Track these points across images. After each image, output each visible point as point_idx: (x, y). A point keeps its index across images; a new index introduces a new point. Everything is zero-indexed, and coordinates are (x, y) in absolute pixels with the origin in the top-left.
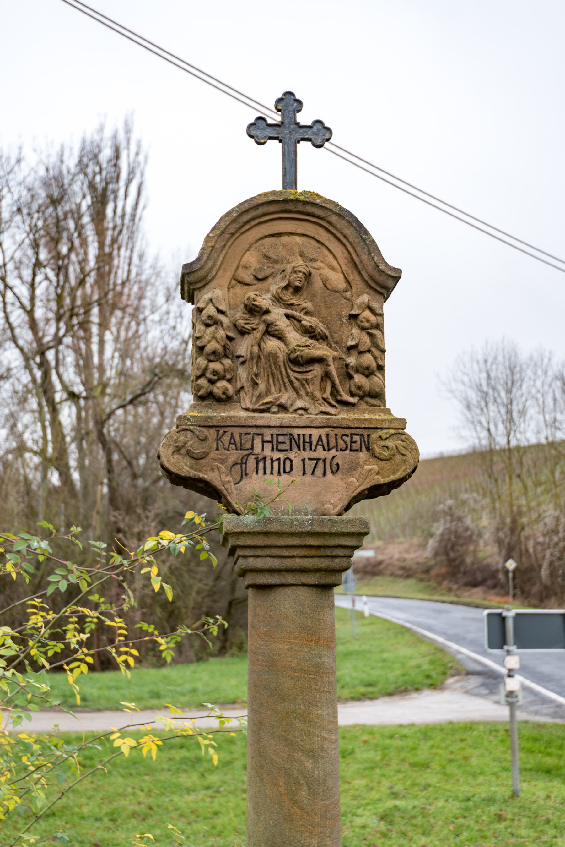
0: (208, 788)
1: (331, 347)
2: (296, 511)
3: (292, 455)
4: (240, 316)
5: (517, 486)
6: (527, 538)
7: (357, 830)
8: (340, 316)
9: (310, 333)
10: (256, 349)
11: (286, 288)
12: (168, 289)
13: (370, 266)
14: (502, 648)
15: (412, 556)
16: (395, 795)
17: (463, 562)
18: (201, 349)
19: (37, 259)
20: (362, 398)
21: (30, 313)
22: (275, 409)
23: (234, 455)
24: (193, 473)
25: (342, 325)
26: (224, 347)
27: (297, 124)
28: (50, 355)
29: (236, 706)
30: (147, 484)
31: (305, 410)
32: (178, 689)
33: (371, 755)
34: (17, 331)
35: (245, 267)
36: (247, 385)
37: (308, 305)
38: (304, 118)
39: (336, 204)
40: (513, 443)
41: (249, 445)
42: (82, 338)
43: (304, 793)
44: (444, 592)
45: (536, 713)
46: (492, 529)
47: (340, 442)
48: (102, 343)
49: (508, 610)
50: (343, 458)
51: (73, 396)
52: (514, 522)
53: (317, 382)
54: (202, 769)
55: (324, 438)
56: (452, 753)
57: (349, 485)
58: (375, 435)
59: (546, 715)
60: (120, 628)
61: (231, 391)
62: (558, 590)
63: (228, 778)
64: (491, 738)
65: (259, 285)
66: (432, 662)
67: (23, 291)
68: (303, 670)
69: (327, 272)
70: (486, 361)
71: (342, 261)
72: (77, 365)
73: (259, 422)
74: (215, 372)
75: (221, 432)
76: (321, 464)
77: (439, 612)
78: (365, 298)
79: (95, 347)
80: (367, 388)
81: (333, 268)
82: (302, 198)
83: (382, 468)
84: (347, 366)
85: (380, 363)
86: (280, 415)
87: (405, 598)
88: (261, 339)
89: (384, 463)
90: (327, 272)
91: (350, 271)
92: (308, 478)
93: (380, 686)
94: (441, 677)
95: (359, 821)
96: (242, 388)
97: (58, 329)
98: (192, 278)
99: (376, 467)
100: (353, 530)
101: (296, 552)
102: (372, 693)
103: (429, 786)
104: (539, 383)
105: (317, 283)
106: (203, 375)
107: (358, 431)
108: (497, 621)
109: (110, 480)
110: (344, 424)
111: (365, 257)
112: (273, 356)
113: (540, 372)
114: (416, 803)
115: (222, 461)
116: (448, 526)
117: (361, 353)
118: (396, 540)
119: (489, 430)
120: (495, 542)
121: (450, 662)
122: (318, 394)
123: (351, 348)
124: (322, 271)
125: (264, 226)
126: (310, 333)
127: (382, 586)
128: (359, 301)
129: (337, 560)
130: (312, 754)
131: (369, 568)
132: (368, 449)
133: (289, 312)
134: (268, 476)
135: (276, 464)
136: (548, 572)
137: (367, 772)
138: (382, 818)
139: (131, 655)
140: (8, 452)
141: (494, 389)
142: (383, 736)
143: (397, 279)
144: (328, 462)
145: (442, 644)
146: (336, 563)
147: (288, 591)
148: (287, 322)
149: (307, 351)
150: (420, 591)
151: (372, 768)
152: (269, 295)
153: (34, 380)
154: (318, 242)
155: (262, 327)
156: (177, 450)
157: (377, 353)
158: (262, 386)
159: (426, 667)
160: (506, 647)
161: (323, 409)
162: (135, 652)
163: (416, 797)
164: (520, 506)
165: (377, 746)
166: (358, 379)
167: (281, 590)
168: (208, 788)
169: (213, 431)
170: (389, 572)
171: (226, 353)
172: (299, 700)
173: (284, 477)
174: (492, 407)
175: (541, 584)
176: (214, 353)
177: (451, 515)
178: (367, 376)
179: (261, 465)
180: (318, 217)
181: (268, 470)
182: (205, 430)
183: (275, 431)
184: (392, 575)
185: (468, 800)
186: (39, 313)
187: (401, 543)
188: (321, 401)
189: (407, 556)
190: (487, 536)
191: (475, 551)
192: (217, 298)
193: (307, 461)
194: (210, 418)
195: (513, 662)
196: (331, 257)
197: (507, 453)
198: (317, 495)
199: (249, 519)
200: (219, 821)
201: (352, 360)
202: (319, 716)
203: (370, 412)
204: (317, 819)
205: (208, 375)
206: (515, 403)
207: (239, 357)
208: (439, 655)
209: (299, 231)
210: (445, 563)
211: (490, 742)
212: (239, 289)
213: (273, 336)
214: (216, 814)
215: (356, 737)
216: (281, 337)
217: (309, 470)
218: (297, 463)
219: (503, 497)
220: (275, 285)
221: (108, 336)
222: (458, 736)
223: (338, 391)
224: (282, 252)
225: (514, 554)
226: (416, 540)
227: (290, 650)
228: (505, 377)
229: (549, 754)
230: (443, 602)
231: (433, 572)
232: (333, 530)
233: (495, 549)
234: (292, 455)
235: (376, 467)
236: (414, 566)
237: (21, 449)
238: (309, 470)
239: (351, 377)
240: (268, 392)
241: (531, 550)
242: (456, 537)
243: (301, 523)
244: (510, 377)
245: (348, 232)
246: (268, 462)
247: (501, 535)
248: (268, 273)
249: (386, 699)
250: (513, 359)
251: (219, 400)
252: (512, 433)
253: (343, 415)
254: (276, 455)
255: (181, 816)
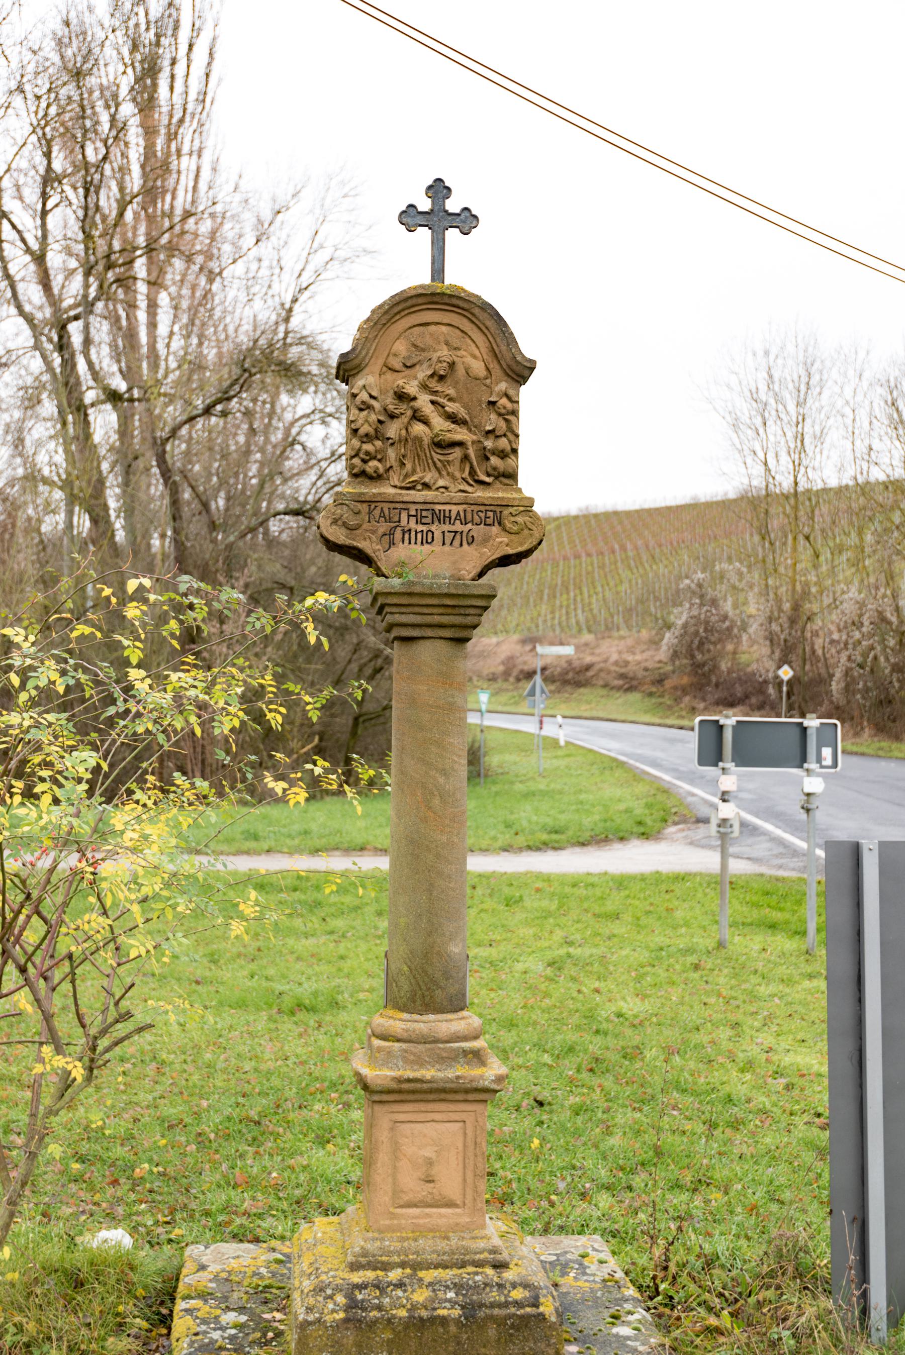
0: (332, 933)
1: (470, 431)
2: (435, 576)
3: (433, 528)
4: (390, 401)
5: (805, 554)
6: (816, 634)
7: (517, 975)
8: (480, 401)
9: (453, 418)
10: (404, 432)
11: (432, 376)
12: (260, 222)
13: (508, 356)
14: (717, 765)
15: (638, 657)
16: (570, 943)
17: (715, 667)
18: (355, 431)
19: (49, 168)
20: (496, 478)
21: (40, 259)
22: (419, 487)
23: (384, 527)
24: (348, 542)
25: (481, 410)
26: (376, 430)
27: (446, 211)
28: (75, 330)
29: (365, 853)
30: (232, 538)
31: (446, 488)
32: (283, 830)
33: (545, 903)
34: (20, 287)
35: (395, 355)
36: (395, 464)
37: (451, 392)
38: (453, 205)
39: (479, 298)
40: (803, 485)
41: (396, 519)
42: (122, 301)
43: (436, 801)
44: (684, 713)
45: (780, 867)
46: (761, 619)
47: (476, 517)
48: (152, 306)
49: (727, 717)
50: (478, 531)
51: (114, 397)
52: (796, 607)
53: (457, 463)
54: (323, 914)
55: (462, 514)
56: (652, 904)
57: (482, 554)
58: (506, 512)
59: (794, 869)
60: (271, 686)
61: (381, 470)
62: (856, 713)
63: (357, 923)
64: (708, 890)
65: (408, 372)
66: (649, 806)
67: (28, 223)
68: (438, 707)
69: (469, 360)
70: (767, 353)
71: (484, 350)
72: (113, 346)
73: (406, 499)
74: (367, 453)
75: (373, 506)
76: (458, 536)
77: (673, 741)
78: (503, 386)
79: (142, 316)
80: (502, 470)
81: (475, 357)
82: (448, 292)
83: (511, 541)
84: (485, 448)
85: (514, 446)
86: (423, 493)
87: (623, 721)
88: (409, 423)
89: (513, 537)
90: (469, 360)
91: (490, 360)
92: (447, 548)
93: (570, 833)
94: (659, 825)
95: (520, 967)
96: (391, 467)
97: (87, 286)
98: (347, 366)
99: (506, 540)
100: (483, 592)
101: (435, 610)
102: (557, 842)
103: (614, 936)
104: (848, 392)
105: (460, 371)
106: (356, 455)
107: (492, 508)
108: (713, 729)
109: (175, 531)
110: (480, 501)
111: (504, 348)
112: (418, 440)
113: (851, 373)
114: (594, 951)
115: (374, 532)
116: (695, 612)
117: (497, 437)
118: (615, 634)
119: (766, 464)
120: (766, 638)
121: (674, 806)
122: (458, 474)
123: (489, 432)
124: (464, 359)
125: (413, 316)
126: (453, 418)
127: (589, 703)
128: (497, 389)
129: (469, 618)
130: (444, 772)
131: (570, 675)
132: (500, 524)
133: (434, 398)
134: (413, 545)
135: (419, 535)
136: (843, 685)
137: (537, 922)
138: (550, 964)
139: (280, 713)
140: (11, 483)
141: (778, 399)
142: (562, 884)
143: (532, 369)
144: (464, 534)
145: (669, 783)
146: (469, 620)
147: (428, 643)
148: (431, 407)
149: (449, 435)
150: (646, 712)
151: (545, 918)
152: (416, 383)
153: (49, 368)
154: (462, 331)
155: (409, 413)
156: (335, 522)
157: (512, 437)
158: (409, 466)
159: (638, 811)
160: (721, 764)
161: (462, 487)
162: (283, 710)
163: (596, 946)
164: (807, 584)
165: (553, 894)
166: (494, 460)
167: (422, 642)
168: (332, 933)
169: (365, 505)
170: (601, 683)
171: (378, 435)
172: (435, 730)
173: (426, 546)
174: (772, 427)
175: (832, 702)
176: (367, 435)
177: (702, 597)
178: (502, 458)
179: (407, 536)
180: (463, 309)
181: (413, 541)
182: (358, 504)
183: (420, 507)
184: (605, 686)
185: (661, 949)
186: (54, 259)
187: (622, 638)
188: (460, 480)
189: (630, 658)
190: (754, 628)
191: (735, 653)
192: (370, 385)
193: (447, 534)
194: (363, 494)
195: (728, 783)
196: (473, 345)
197: (792, 501)
198: (454, 563)
199: (395, 583)
200: (346, 965)
201: (489, 444)
202: (450, 744)
203: (503, 491)
204: (447, 822)
205: (361, 455)
206: (808, 421)
207: (388, 439)
208: (661, 797)
209: (445, 321)
210: (689, 668)
211: (706, 895)
212: (389, 376)
213: (419, 420)
214: (342, 958)
215: (526, 884)
216: (426, 422)
217: (448, 541)
218: (438, 535)
219: (782, 570)
220: (422, 373)
221: (163, 299)
222: (664, 887)
223: (475, 472)
224: (429, 341)
225: (793, 657)
226: (645, 634)
227: (428, 690)
228: (796, 378)
229: (781, 910)
230: (681, 728)
231: (668, 684)
232: (466, 592)
233: (766, 651)
234: (433, 528)
235: (506, 540)
236: (640, 674)
237: (33, 478)
238: (448, 541)
239: (488, 459)
240: (414, 472)
241: (819, 652)
242: (706, 630)
243: (440, 586)
244: (804, 379)
245: (489, 323)
246: (413, 534)
247: (775, 627)
248: (415, 360)
249: (578, 850)
250: (810, 349)
251: (371, 478)
252: (802, 470)
253: (480, 493)
254: (420, 528)
255: (298, 959)
